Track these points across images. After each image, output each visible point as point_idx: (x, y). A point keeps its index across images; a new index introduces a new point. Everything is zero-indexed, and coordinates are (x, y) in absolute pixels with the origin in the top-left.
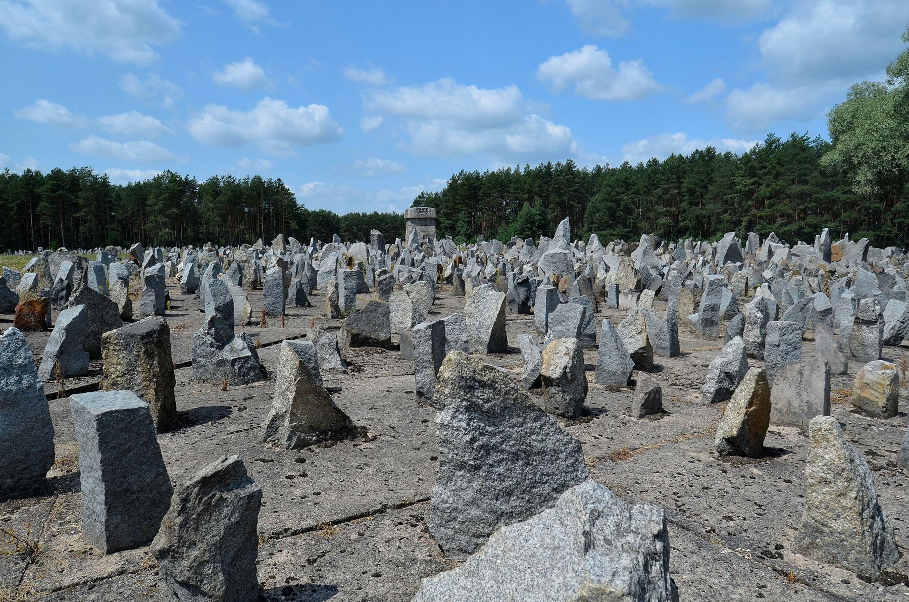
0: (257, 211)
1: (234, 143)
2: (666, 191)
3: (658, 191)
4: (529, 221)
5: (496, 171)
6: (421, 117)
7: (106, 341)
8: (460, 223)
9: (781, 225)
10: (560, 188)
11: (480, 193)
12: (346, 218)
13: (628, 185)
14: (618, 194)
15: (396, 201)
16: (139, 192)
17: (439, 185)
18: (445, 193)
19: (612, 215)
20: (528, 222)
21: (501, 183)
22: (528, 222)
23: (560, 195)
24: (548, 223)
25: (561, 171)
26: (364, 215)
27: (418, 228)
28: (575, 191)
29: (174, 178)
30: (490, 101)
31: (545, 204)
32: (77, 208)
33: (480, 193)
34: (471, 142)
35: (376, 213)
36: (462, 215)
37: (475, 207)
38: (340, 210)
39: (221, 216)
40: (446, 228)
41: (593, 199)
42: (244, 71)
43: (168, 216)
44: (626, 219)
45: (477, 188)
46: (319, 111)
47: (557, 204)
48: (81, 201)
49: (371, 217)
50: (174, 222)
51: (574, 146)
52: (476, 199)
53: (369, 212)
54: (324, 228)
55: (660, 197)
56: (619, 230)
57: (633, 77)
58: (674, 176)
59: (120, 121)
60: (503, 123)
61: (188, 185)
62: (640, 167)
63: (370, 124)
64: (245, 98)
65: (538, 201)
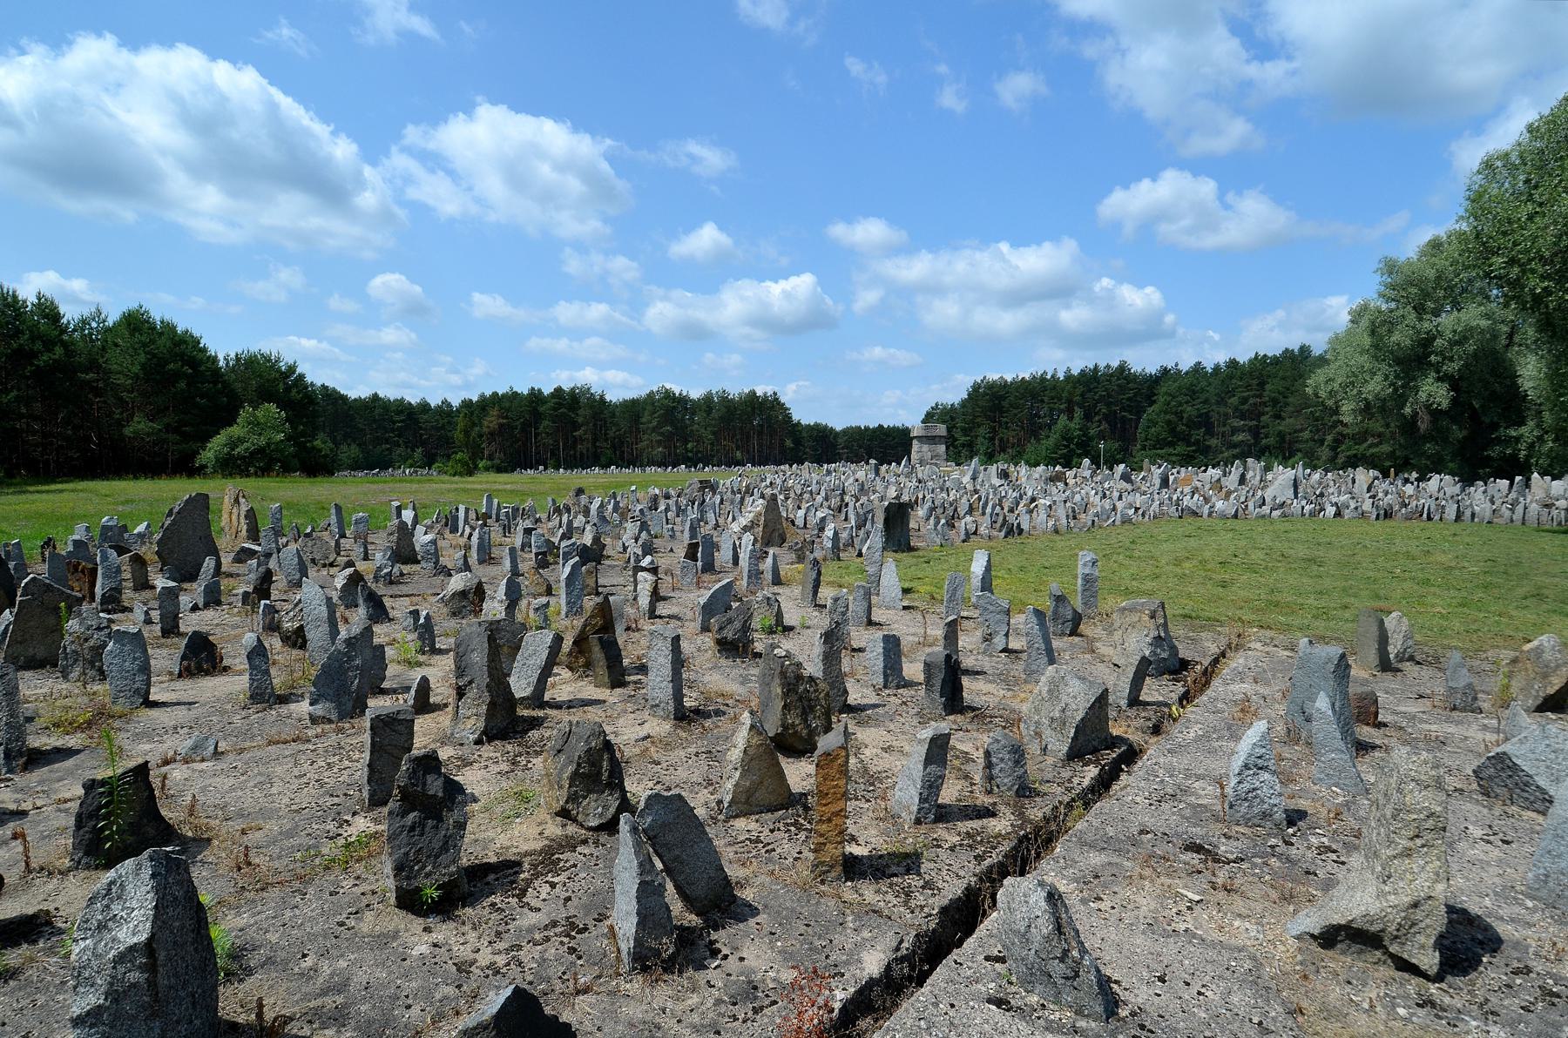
0: (753, 431)
1: (695, 334)
2: (1244, 401)
3: (1234, 401)
4: (1066, 437)
5: (1027, 377)
6: (935, 289)
7: (1454, 383)
8: (980, 440)
9: (1370, 446)
10: (1109, 396)
11: (1005, 404)
12: (846, 432)
13: (1194, 392)
14: (1180, 404)
15: (903, 410)
16: (633, 408)
17: (954, 393)
18: (964, 403)
19: (1173, 431)
20: (1064, 438)
21: (1037, 392)
22: (1064, 438)
23: (1108, 404)
24: (1091, 439)
25: (1111, 375)
26: (867, 429)
27: (925, 448)
28: (1129, 399)
29: (668, 394)
30: (1034, 262)
31: (1088, 417)
32: (576, 426)
33: (1005, 404)
34: (1008, 321)
35: (881, 426)
36: (982, 431)
37: (997, 421)
38: (838, 422)
39: (714, 433)
40: (963, 445)
41: (1150, 410)
42: (707, 237)
43: (662, 434)
44: (1190, 435)
45: (1003, 398)
46: (803, 283)
47: (1106, 417)
48: (580, 420)
49: (874, 430)
50: (668, 440)
51: (1169, 319)
52: (1000, 409)
53: (873, 425)
54: (823, 446)
55: (1236, 409)
56: (1180, 449)
57: (1254, 216)
58: (1255, 382)
59: (566, 312)
60: (1059, 291)
61: (682, 401)
62: (1217, 368)
63: (869, 297)
64: (708, 277)
65: (1078, 413)
